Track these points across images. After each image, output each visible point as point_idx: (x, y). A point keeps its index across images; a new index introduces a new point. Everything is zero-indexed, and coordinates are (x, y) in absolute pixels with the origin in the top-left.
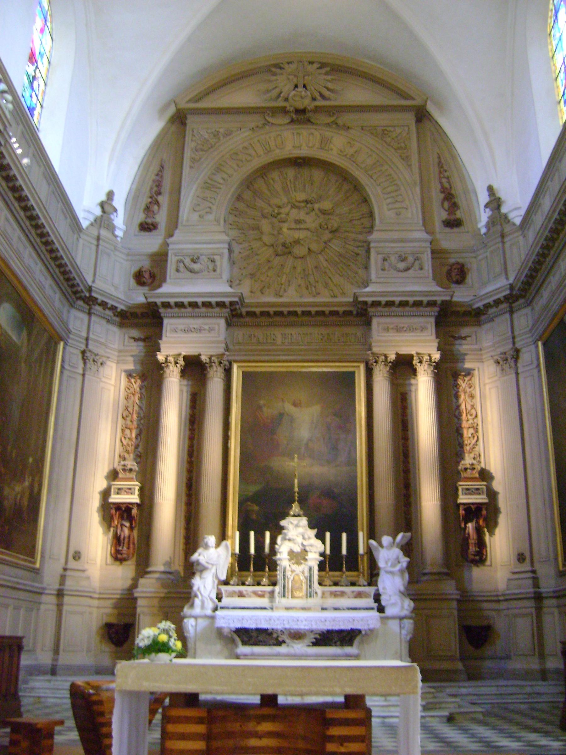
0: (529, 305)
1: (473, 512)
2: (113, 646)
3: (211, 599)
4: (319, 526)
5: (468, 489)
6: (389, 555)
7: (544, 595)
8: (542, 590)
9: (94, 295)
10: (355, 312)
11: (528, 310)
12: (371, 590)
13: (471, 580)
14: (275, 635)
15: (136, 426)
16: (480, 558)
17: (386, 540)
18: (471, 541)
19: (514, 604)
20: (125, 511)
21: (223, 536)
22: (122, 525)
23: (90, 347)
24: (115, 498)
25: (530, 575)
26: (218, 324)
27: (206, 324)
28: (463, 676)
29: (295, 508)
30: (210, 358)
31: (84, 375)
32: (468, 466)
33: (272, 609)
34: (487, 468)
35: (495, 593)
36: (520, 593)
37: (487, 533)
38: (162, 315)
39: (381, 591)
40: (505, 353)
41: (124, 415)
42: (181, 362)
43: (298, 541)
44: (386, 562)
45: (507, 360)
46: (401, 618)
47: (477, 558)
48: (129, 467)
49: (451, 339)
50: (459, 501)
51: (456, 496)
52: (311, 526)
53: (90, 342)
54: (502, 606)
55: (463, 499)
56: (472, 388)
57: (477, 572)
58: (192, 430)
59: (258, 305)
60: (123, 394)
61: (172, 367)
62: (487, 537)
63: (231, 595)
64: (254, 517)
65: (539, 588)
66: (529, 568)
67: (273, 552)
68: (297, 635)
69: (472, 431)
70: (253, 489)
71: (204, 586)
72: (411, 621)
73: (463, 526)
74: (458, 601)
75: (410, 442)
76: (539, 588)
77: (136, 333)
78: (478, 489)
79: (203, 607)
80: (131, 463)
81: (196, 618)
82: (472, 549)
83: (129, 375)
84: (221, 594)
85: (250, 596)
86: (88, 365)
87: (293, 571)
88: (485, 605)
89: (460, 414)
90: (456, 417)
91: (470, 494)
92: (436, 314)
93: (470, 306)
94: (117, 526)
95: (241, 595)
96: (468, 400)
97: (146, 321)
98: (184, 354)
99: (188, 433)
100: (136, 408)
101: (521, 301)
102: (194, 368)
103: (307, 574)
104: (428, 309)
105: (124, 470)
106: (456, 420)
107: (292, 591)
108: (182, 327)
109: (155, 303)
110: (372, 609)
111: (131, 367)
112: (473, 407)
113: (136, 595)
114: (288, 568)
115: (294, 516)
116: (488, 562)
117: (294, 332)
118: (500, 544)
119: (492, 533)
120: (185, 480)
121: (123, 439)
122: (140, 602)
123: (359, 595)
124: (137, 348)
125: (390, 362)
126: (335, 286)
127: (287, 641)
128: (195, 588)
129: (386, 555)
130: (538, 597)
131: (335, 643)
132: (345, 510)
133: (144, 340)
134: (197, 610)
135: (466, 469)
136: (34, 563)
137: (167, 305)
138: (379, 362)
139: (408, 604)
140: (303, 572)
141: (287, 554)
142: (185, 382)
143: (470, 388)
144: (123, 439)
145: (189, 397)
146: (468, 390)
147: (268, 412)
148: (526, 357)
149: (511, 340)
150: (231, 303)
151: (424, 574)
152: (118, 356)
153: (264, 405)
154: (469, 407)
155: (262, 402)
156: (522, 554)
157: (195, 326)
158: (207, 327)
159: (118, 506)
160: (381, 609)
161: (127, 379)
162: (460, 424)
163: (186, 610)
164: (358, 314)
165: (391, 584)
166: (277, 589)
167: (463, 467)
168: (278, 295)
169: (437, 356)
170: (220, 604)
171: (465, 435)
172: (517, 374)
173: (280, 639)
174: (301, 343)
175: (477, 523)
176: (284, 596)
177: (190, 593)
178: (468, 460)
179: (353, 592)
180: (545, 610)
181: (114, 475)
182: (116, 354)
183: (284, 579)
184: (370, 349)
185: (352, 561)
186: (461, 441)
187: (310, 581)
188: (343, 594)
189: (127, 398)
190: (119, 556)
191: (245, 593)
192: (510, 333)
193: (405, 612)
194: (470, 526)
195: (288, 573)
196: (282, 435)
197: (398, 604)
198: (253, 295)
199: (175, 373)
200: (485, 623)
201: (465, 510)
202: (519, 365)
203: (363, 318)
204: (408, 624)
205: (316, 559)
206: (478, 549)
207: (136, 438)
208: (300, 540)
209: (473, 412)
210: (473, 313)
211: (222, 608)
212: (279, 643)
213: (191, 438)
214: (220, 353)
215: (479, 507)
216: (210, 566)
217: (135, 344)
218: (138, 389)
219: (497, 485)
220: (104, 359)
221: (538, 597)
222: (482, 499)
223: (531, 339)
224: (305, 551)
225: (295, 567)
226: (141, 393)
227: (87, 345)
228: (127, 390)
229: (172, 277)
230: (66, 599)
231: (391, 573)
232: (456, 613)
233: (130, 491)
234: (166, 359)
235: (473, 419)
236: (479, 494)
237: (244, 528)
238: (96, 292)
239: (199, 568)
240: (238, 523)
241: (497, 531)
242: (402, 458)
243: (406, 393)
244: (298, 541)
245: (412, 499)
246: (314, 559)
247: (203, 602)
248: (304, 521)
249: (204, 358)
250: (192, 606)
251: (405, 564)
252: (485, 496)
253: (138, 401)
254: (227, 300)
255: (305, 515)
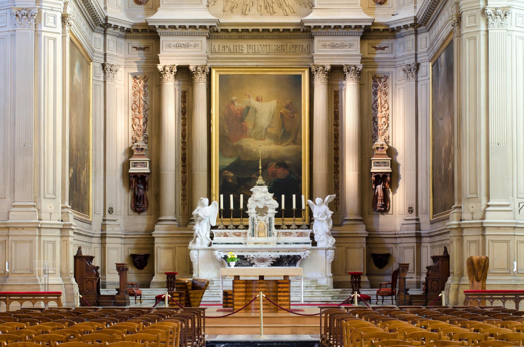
0: (428, 31)
1: (380, 178)
2: (137, 269)
3: (207, 238)
4: (276, 190)
5: (378, 163)
6: (321, 210)
7: (423, 235)
8: (422, 232)
9: (109, 22)
10: (302, 30)
11: (426, 34)
12: (309, 231)
13: (378, 225)
14: (248, 260)
15: (143, 116)
16: (385, 209)
17: (318, 200)
18: (379, 198)
19: (404, 240)
20: (141, 178)
21: (209, 196)
22: (139, 188)
23: (108, 60)
24: (133, 170)
25: (415, 222)
26: (201, 41)
27: (192, 41)
28: (368, 285)
29: (260, 180)
30: (196, 68)
31: (105, 82)
32: (379, 146)
33: (246, 244)
34: (393, 147)
35: (394, 233)
36: (408, 234)
37: (391, 192)
38: (159, 34)
39: (314, 232)
40: (410, 65)
41: (133, 108)
42: (175, 70)
43: (261, 196)
44: (318, 215)
45: (410, 70)
46: (327, 249)
47: (383, 209)
48: (141, 147)
49: (374, 49)
50: (372, 171)
51: (370, 167)
52: (270, 191)
53: (107, 56)
54: (399, 241)
55: (374, 169)
56: (387, 87)
57: (382, 218)
58: (184, 119)
59: (230, 24)
60: (131, 92)
61: (168, 74)
62: (391, 195)
63: (219, 235)
64: (230, 181)
65: (420, 230)
66: (415, 217)
67: (246, 208)
68: (263, 260)
69: (384, 119)
70: (228, 162)
71: (202, 230)
72: (333, 251)
73: (374, 187)
74: (367, 238)
75: (340, 127)
76: (420, 230)
77: (137, 43)
78: (385, 162)
79: (202, 243)
80: (141, 143)
81: (198, 250)
82: (379, 203)
83: (135, 77)
84: (213, 235)
85: (232, 236)
86: (107, 75)
87: (258, 220)
88: (387, 241)
89: (377, 107)
90: (374, 109)
91: (380, 166)
92: (361, 34)
93: (388, 26)
94: (135, 188)
95: (226, 235)
96: (383, 96)
97: (148, 37)
98: (177, 65)
99: (181, 121)
100: (142, 102)
101: (422, 28)
102: (184, 73)
103: (268, 222)
104: (356, 30)
105: (137, 149)
106: (373, 112)
107: (258, 233)
108: (175, 43)
109: (154, 26)
110: (309, 243)
111: (136, 70)
112: (386, 101)
113: (153, 236)
114: (255, 218)
115: (259, 185)
116: (390, 212)
117: (256, 43)
118: (399, 199)
119: (394, 192)
120: (181, 155)
121: (134, 126)
122: (156, 240)
123: (301, 235)
124: (139, 56)
125: (326, 71)
126: (288, 6)
127: (256, 263)
128: (196, 232)
129: (318, 210)
130: (419, 237)
131: (286, 264)
132: (293, 176)
133: (144, 49)
134: (198, 245)
135: (378, 148)
136: (89, 218)
137: (164, 27)
138: (319, 71)
139: (332, 240)
140: (265, 221)
141: (254, 209)
142: (177, 83)
143: (385, 87)
144: (134, 126)
145: (181, 94)
146: (383, 89)
147: (239, 106)
148: (422, 70)
149: (414, 56)
150: (210, 27)
151: (346, 220)
152: (125, 62)
153: (236, 100)
154: (383, 102)
155: (234, 98)
156: (411, 208)
157: (184, 43)
158: (192, 44)
159: (135, 175)
160: (314, 244)
161: (133, 80)
162: (376, 114)
163: (191, 245)
164: (304, 31)
165: (322, 227)
166: (249, 231)
167: (376, 147)
168: (244, 14)
169: (360, 67)
170: (213, 242)
171: (379, 123)
172: (417, 82)
173: (252, 262)
174: (261, 53)
175: (384, 185)
176: (253, 236)
177: (193, 234)
178: (380, 142)
179: (297, 233)
180: (423, 244)
181: (130, 152)
182: (124, 60)
183: (253, 225)
184: (313, 62)
185: (299, 213)
186: (376, 127)
187: (270, 226)
188: (290, 234)
189: (134, 95)
190: (138, 209)
191: (228, 234)
192: (414, 51)
193: (330, 246)
194: (380, 187)
195: (256, 222)
196: (249, 123)
197: (325, 241)
198: (225, 13)
199: (171, 79)
200: (386, 252)
201: (375, 176)
202: (419, 75)
203: (308, 34)
204: (331, 253)
205: (273, 213)
206: (383, 203)
207: (144, 125)
208: (263, 201)
209: (386, 105)
210: (390, 30)
211: (214, 244)
212: (252, 265)
213: (184, 125)
214: (203, 64)
215: (385, 175)
216: (206, 218)
217: (137, 52)
218: (142, 88)
219: (400, 159)
220: (117, 67)
221: (419, 237)
222: (387, 169)
223: (428, 57)
224: (266, 208)
225: (259, 218)
226: (145, 91)
227: (105, 59)
228: (134, 88)
229: (164, 3)
230: (108, 240)
231: (322, 221)
232: (365, 245)
233: (143, 164)
234: (164, 69)
235: (386, 111)
236: (386, 166)
237: (225, 189)
238: (110, 20)
239: (199, 219)
240: (219, 185)
241: (398, 190)
242: (333, 139)
243: (338, 92)
244: (261, 196)
245: (340, 168)
246: (272, 212)
247: (202, 240)
248: (265, 188)
249: (192, 68)
250: (195, 242)
251: (330, 216)
252: (390, 168)
253: (143, 97)
254: (208, 25)
255: (266, 184)
